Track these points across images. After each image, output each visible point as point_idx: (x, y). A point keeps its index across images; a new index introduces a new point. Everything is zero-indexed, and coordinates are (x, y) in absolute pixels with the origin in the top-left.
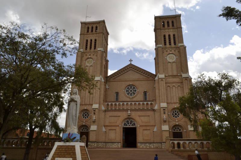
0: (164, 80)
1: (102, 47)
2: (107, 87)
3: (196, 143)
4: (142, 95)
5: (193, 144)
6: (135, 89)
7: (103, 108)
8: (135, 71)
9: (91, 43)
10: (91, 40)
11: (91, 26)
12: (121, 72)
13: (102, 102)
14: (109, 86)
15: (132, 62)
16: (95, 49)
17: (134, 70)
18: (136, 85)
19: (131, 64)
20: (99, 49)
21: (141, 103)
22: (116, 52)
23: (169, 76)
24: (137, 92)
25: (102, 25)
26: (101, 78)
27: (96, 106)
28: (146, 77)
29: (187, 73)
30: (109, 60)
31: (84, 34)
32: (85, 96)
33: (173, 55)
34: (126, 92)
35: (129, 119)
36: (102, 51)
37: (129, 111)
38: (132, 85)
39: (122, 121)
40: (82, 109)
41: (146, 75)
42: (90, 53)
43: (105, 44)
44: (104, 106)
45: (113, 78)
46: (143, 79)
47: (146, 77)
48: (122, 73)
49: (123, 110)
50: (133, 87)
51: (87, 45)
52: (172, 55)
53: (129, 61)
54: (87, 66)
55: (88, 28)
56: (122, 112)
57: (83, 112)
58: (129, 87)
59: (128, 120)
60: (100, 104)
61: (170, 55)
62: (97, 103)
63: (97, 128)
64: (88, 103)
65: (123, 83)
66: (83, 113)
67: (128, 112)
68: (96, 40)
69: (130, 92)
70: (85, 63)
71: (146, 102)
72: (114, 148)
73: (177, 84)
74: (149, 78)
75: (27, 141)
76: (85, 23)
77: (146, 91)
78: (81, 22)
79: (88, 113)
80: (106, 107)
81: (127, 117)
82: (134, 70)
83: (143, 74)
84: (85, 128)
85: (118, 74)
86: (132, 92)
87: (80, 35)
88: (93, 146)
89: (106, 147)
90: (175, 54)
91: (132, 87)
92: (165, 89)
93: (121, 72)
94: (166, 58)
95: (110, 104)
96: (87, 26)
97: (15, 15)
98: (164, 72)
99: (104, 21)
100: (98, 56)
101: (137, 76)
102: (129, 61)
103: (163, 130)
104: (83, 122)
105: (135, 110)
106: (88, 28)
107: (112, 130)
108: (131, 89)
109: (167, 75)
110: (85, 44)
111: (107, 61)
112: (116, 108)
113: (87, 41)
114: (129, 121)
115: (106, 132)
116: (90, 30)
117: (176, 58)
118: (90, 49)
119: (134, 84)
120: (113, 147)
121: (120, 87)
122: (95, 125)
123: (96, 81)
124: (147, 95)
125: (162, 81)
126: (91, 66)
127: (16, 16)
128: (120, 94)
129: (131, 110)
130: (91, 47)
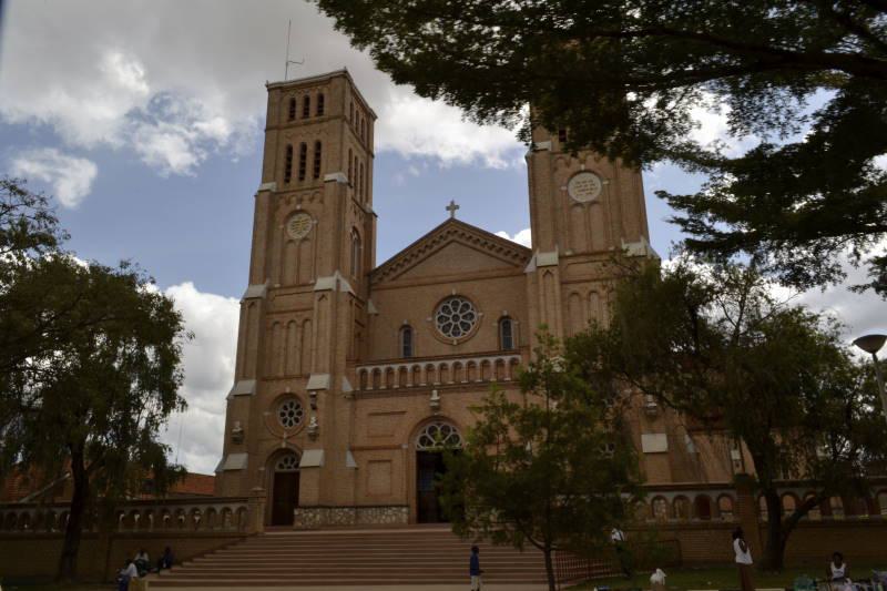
0: (555, 271)
1: (340, 169)
2: (372, 309)
3: (680, 497)
4: (496, 331)
5: (671, 501)
6: (470, 311)
7: (347, 387)
8: (466, 245)
9: (303, 157)
10: (304, 147)
11: (303, 95)
12: (420, 251)
13: (342, 361)
14: (377, 308)
15: (456, 211)
16: (316, 177)
17: (470, 243)
18: (470, 297)
19: (452, 221)
20: (328, 177)
21: (492, 360)
22: (496, 167)
23: (575, 255)
24: (475, 319)
25: (340, 89)
26: (338, 281)
27: (319, 381)
28: (509, 263)
29: (642, 239)
30: (376, 212)
31: (278, 128)
32: (286, 349)
33: (591, 176)
34: (437, 323)
35: (436, 421)
36: (341, 184)
37: (435, 392)
38: (458, 296)
39: (411, 427)
40: (278, 394)
41: (509, 258)
42: (299, 194)
43: (359, 153)
44: (349, 380)
45: (393, 275)
46: (494, 274)
47: (509, 263)
48: (421, 256)
49: (416, 390)
50: (461, 304)
51: (289, 167)
52: (588, 175)
53: (448, 208)
54: (291, 241)
55: (293, 103)
56: (411, 398)
57: (279, 403)
58: (450, 305)
59: (433, 424)
60: (334, 373)
61: (582, 175)
62: (324, 372)
63: (668, 440)
64: (297, 372)
65: (427, 289)
66: (282, 406)
67: (431, 395)
68: (318, 145)
69: (454, 323)
70: (285, 229)
71: (410, 362)
72: (387, 526)
73: (586, 284)
74: (517, 266)
75: (65, 514)
76: (280, 88)
77: (508, 317)
78: (267, 86)
79: (298, 407)
80: (358, 381)
81: (428, 414)
82: (463, 241)
83: (495, 254)
84: (290, 459)
85: (409, 261)
86: (461, 320)
87: (266, 130)
88: (310, 520)
89: (360, 522)
90: (599, 172)
91: (447, 307)
92: (558, 307)
93: (420, 251)
94: (564, 188)
95: (370, 369)
96: (287, 98)
97: (129, 66)
98: (556, 241)
99: (346, 72)
100: (327, 201)
101: (476, 262)
102: (448, 208)
103: (645, 450)
104: (281, 438)
105: (459, 388)
106: (293, 103)
107: (379, 461)
108: (455, 311)
109: (568, 253)
110: (282, 164)
111: (369, 218)
112: (406, 380)
113: (290, 150)
114: (439, 429)
115: (356, 469)
116: (299, 109)
117: (603, 186)
118: (302, 179)
119: (465, 294)
120: (382, 522)
121: (416, 305)
122: (319, 448)
123: (321, 293)
124: (512, 330)
125: (548, 276)
126: (305, 239)
127: (134, 70)
128: (415, 332)
129: (443, 389)
130: (303, 172)
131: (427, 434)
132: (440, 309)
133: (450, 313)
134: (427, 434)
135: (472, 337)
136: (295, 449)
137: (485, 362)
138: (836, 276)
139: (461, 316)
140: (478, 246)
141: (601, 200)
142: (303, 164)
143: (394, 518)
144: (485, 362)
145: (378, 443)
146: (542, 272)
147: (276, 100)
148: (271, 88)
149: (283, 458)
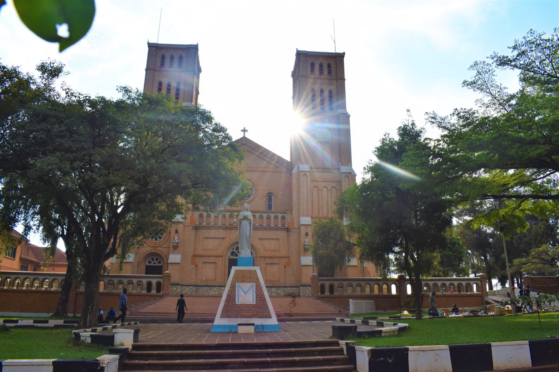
15: (246, 133)
19: (244, 138)
53: (242, 131)
131: (235, 250)
134: (235, 250)
136: (163, 255)
138: (292, 305)
143: (217, 292)
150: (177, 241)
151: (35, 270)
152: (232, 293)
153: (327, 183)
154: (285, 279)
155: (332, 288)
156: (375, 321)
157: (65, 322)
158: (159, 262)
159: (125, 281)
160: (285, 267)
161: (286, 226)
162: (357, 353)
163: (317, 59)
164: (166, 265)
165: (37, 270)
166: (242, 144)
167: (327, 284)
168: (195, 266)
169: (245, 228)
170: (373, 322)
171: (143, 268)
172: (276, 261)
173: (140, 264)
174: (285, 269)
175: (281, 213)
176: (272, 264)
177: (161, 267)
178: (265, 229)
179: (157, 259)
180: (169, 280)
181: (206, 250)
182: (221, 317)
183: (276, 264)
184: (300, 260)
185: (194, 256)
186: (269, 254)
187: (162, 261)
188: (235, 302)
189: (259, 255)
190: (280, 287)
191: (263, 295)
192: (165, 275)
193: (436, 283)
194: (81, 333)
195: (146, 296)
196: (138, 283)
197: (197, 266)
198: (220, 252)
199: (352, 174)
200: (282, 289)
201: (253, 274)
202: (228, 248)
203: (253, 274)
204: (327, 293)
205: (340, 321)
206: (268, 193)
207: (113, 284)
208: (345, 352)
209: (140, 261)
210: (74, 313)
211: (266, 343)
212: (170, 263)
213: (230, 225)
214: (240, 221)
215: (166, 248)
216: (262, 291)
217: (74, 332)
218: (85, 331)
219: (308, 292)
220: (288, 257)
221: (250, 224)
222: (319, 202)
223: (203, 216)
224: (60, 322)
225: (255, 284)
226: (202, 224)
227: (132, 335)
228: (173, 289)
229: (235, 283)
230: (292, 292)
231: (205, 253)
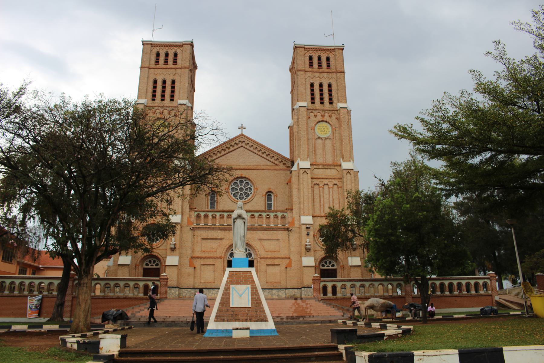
10: (164, 82)
16: (172, 100)
20: (180, 102)
50: (245, 182)
55: (158, 55)
58: (238, 182)
68: (173, 82)
76: (151, 44)
78: (142, 42)
82: (247, 147)
86: (243, 192)
96: (155, 51)
106: (158, 55)
110: (150, 90)
113: (155, 82)
116: (162, 58)
118: (163, 100)
119: (247, 177)
125: (305, 173)
130: (163, 96)
132: (232, 184)
133: (241, 185)
135: (250, 201)
136: (161, 258)
137: (260, 215)
139: (244, 188)
140: (256, 151)
141: (331, 137)
142: (163, 91)
144: (253, 215)
145: (206, 255)
146: (302, 171)
147: (149, 51)
148: (144, 43)
149: (148, 260)
150: (174, 243)
151: (33, 274)
152: (226, 295)
153: (328, 180)
154: (286, 281)
155: (334, 288)
156: (378, 324)
157: (60, 327)
158: (157, 265)
159: (122, 284)
160: (286, 268)
161: (287, 225)
162: (357, 358)
163: (315, 52)
164: (164, 267)
165: (36, 274)
166: (240, 141)
167: (330, 285)
168: (193, 268)
169: (239, 227)
170: (376, 325)
171: (141, 271)
172: (276, 262)
173: (137, 266)
174: (286, 270)
175: (281, 212)
176: (272, 265)
177: (158, 270)
178: (265, 229)
179: (154, 262)
180: (167, 282)
181: (204, 251)
182: (215, 321)
183: (276, 265)
184: (302, 261)
185: (191, 258)
186: (270, 255)
187: (159, 264)
188: (230, 306)
189: (259, 256)
190: (281, 289)
191: (259, 297)
192: (162, 277)
193: (443, 283)
194: (67, 339)
195: (143, 299)
196: (136, 287)
197: (195, 268)
198: (218, 254)
199: (354, 170)
200: (283, 291)
201: (249, 276)
202: (227, 249)
203: (249, 276)
204: (330, 294)
205: (342, 323)
206: (268, 192)
207: (109, 287)
208: (345, 358)
209: (138, 264)
210: (71, 317)
211: (259, 348)
212: (167, 265)
213: (228, 225)
214: (234, 220)
215: (164, 250)
216: (258, 293)
217: (61, 338)
218: (74, 337)
219: (310, 294)
220: (289, 258)
221: (245, 223)
222: (320, 201)
223: (200, 217)
224: (56, 327)
225: (249, 286)
226: (199, 225)
227: (118, 342)
228: (171, 292)
229: (230, 286)
230: (294, 293)
231: (203, 255)
